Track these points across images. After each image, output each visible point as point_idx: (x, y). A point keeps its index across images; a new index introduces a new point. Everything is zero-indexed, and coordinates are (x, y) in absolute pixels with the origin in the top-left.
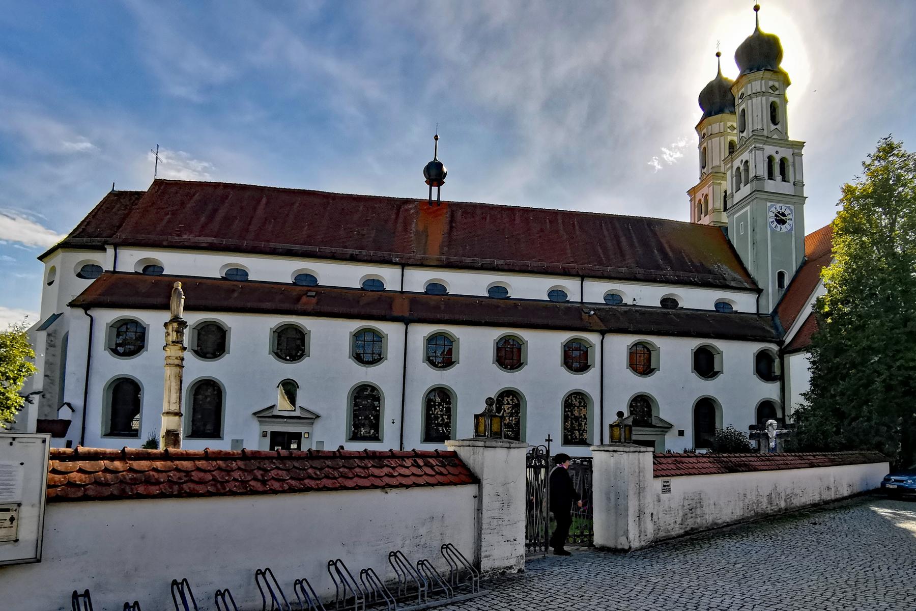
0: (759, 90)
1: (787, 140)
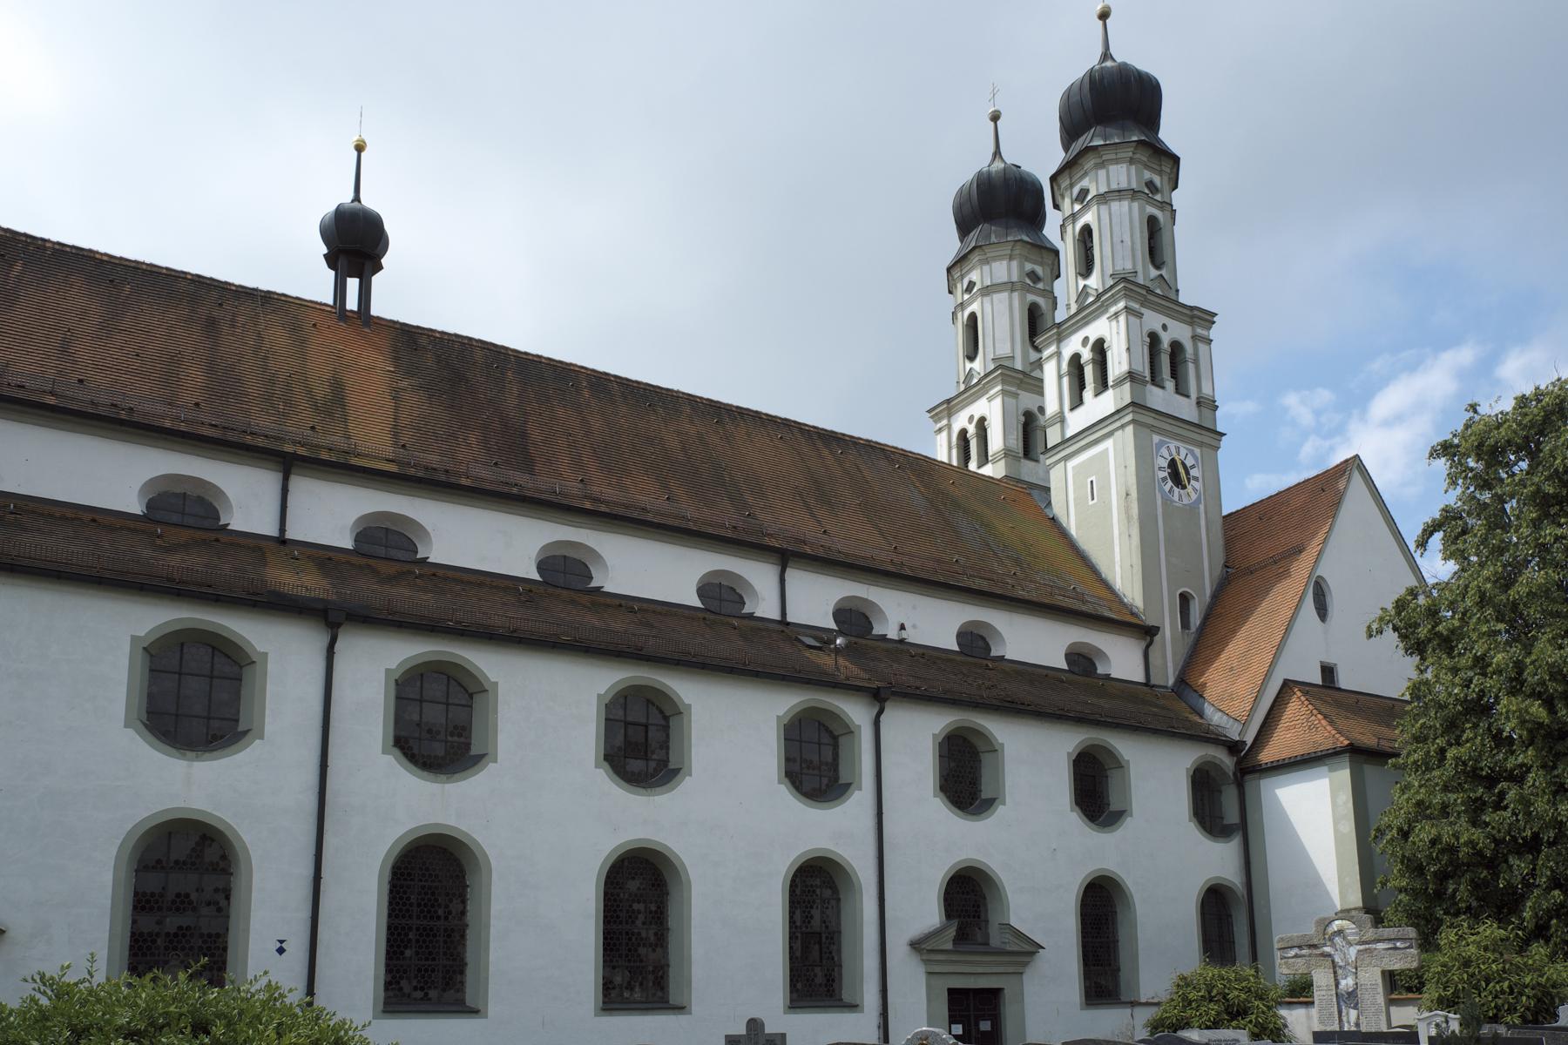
0: (1124, 185)
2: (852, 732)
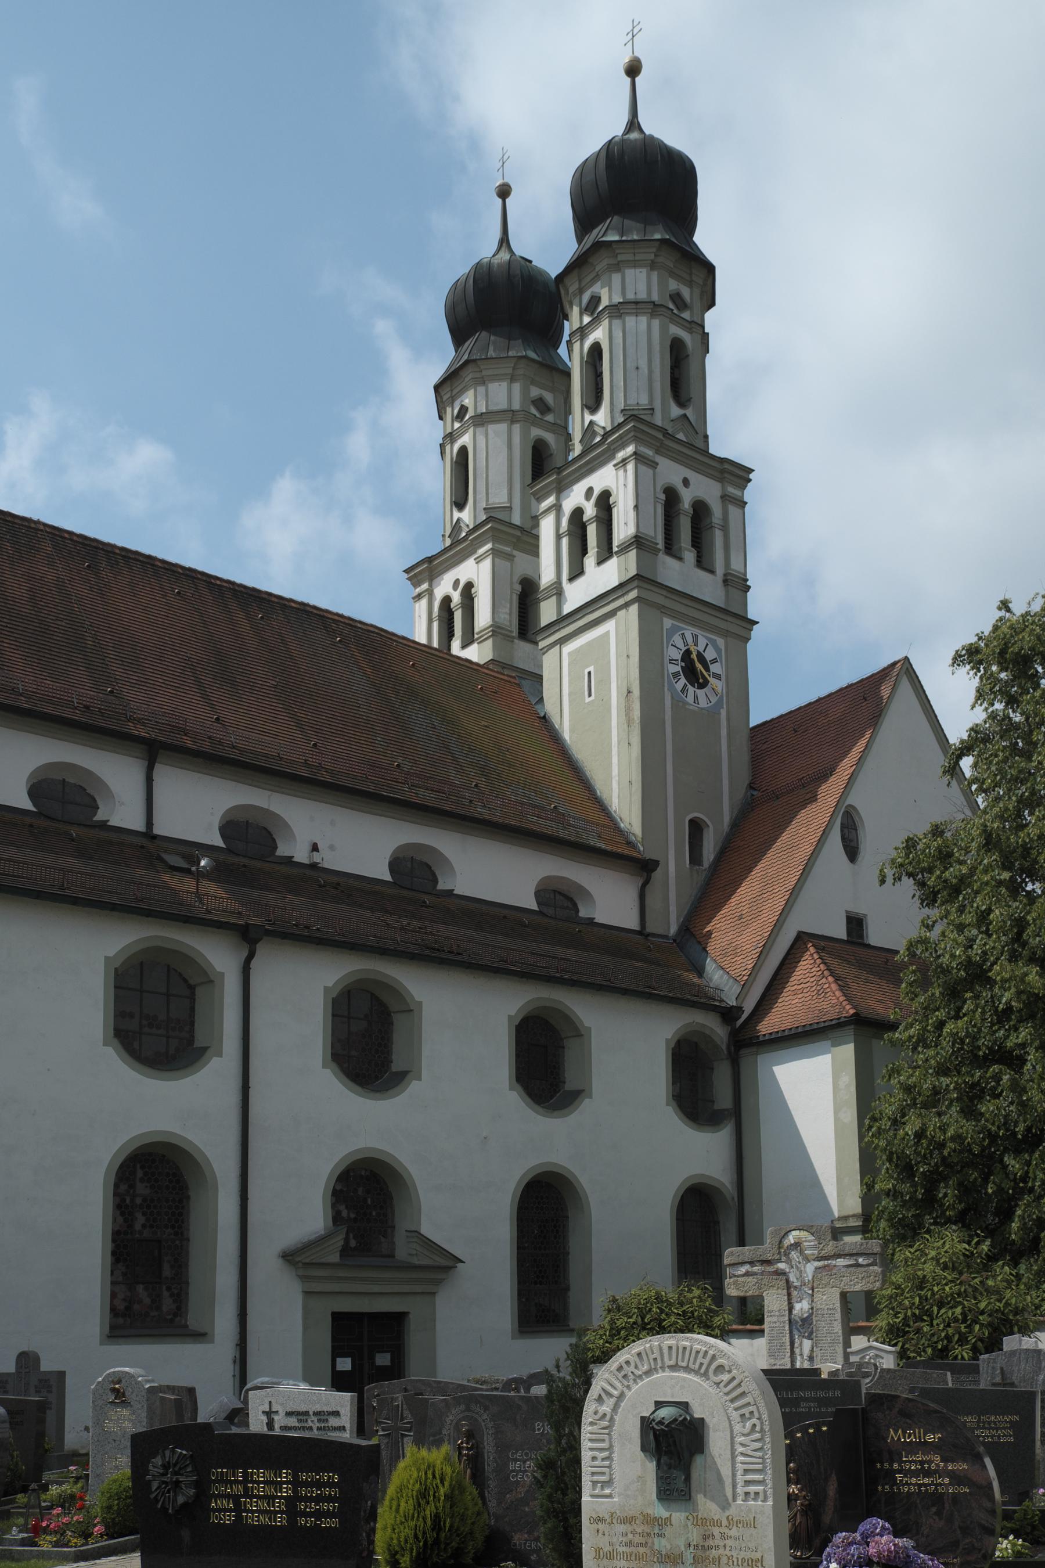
0: (642, 295)
1: (705, 452)
2: (212, 982)
